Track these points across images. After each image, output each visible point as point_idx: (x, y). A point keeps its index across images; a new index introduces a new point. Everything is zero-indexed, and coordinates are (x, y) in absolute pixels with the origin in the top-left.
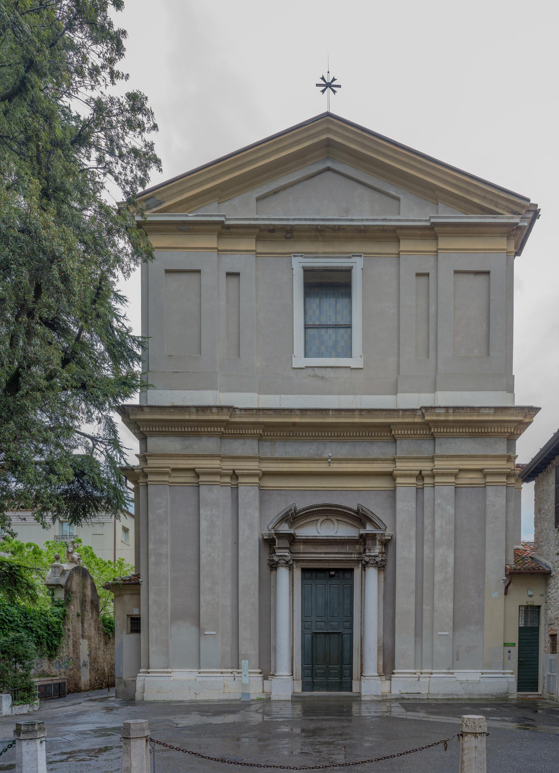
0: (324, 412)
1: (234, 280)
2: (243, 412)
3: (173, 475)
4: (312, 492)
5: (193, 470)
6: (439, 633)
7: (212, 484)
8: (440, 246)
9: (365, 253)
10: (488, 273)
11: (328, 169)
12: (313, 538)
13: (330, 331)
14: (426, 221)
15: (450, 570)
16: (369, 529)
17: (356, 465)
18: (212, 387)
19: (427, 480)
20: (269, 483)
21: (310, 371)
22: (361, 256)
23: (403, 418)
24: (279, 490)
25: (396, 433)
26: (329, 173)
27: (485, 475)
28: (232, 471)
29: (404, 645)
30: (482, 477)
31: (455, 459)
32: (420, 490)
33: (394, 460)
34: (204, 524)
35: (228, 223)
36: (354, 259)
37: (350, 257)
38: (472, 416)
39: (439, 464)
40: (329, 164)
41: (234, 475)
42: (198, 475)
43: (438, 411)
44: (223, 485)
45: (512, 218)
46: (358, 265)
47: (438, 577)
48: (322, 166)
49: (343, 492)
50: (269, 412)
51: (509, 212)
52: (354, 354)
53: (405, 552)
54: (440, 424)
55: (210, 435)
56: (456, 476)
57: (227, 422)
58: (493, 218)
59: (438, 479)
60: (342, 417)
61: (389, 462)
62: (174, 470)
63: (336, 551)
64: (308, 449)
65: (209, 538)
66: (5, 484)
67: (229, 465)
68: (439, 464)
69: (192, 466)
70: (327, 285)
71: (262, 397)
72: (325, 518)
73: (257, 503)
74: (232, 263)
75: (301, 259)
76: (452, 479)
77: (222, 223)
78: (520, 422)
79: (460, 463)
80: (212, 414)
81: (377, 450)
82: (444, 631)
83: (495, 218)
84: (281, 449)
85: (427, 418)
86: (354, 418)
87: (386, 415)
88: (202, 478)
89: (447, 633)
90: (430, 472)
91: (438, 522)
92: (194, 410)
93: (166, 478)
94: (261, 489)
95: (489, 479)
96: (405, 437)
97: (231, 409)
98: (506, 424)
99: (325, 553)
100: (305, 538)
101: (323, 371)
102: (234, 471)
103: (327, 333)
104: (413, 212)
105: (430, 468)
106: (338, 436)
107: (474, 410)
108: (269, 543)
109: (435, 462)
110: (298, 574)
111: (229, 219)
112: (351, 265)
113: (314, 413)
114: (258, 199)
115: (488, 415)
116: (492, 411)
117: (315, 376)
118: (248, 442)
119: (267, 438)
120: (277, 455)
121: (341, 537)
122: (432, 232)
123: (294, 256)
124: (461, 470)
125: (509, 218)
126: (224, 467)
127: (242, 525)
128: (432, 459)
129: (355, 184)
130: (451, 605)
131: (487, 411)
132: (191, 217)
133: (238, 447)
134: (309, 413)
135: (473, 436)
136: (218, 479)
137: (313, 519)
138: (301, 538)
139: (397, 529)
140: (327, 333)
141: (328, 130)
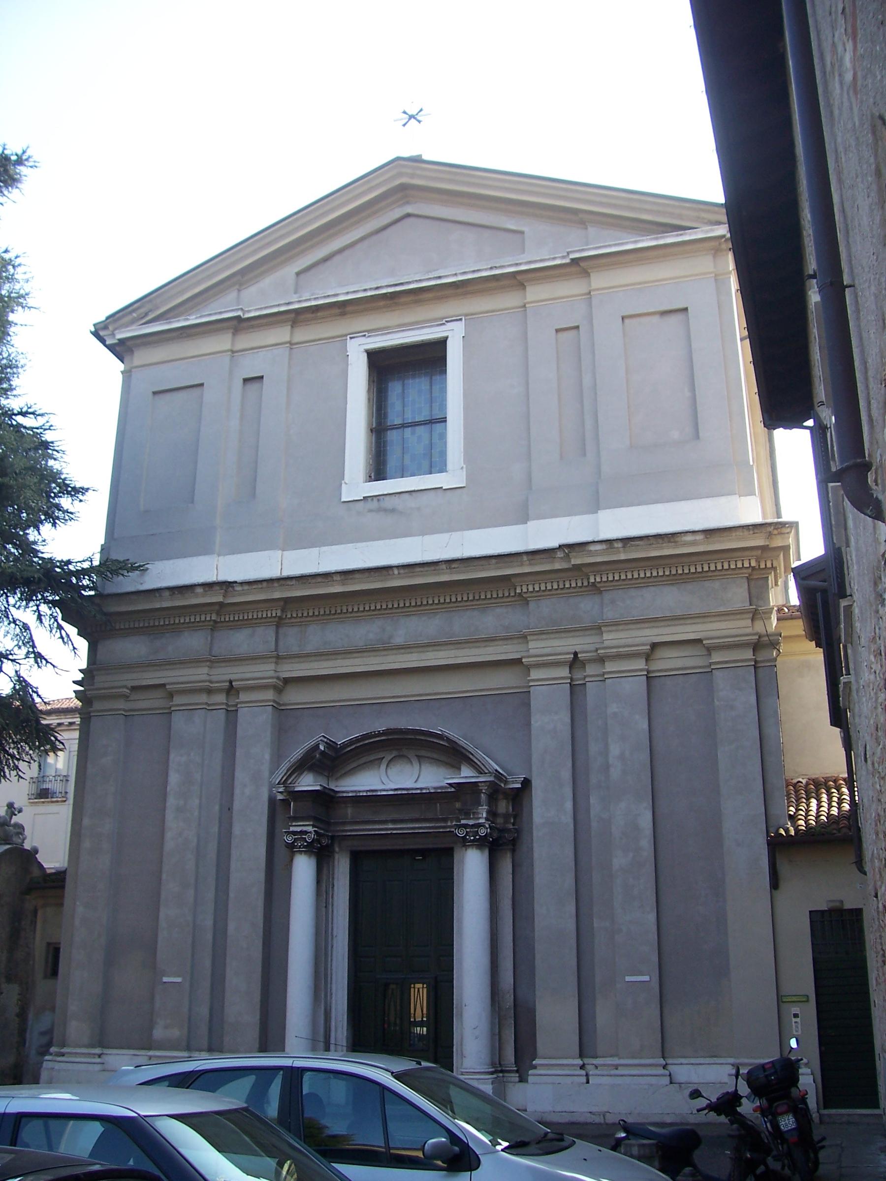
0: (384, 572)
1: (253, 387)
2: (246, 587)
3: (134, 696)
4: (374, 706)
5: (699, 641)
6: (628, 979)
7: (191, 709)
8: (594, 285)
9: (466, 315)
10: (686, 309)
11: (408, 215)
12: (369, 794)
13: (420, 430)
14: (563, 257)
15: (646, 843)
16: (466, 774)
17: (453, 653)
18: (205, 549)
19: (591, 670)
20: (296, 697)
21: (374, 504)
22: (461, 319)
23: (530, 564)
24: (314, 710)
25: (525, 590)
26: (411, 219)
27: (709, 650)
28: (228, 684)
29: (555, 1015)
30: (705, 653)
31: (643, 625)
32: (576, 690)
33: (524, 638)
34: (569, 805)
35: (247, 316)
36: (450, 326)
37: (444, 324)
38: (662, 548)
39: (612, 639)
40: (409, 209)
41: (231, 689)
42: (171, 695)
43: (592, 548)
44: (209, 708)
45: (712, 230)
46: (456, 337)
47: (619, 861)
48: (397, 213)
49: (623, 679)
50: (289, 582)
51: (706, 223)
52: (450, 466)
53: (548, 812)
54: (603, 568)
55: (194, 627)
56: (126, 697)
57: (221, 605)
58: (677, 235)
59: (610, 667)
60: (419, 576)
61: (515, 641)
62: (134, 688)
63: (416, 815)
64: (363, 632)
65: (182, 802)
66: (393, 986)
67: (223, 674)
68: (612, 639)
69: (162, 681)
70: (406, 368)
71: (290, 555)
72: (395, 753)
73: (267, 736)
74: (251, 366)
75: (363, 340)
76: (640, 664)
77: (238, 317)
78: (764, 548)
79: (655, 631)
80: (197, 595)
81: (489, 621)
82: (641, 974)
83: (681, 235)
84: (317, 636)
85: (573, 562)
86: (439, 574)
87: (497, 563)
88: (178, 700)
89: (647, 978)
90: (595, 654)
91: (615, 750)
92: (167, 594)
93: (121, 704)
94: (279, 709)
95: (716, 657)
96: (540, 595)
97: (227, 585)
98: (739, 554)
99: (394, 821)
100: (354, 794)
101: (395, 500)
102: (231, 682)
103: (413, 433)
104: (543, 247)
105: (592, 647)
106: (416, 606)
107: (663, 539)
108: (284, 806)
109: (604, 635)
110: (342, 867)
111: (249, 311)
112: (444, 334)
113: (367, 574)
114: (298, 274)
115: (694, 543)
116: (700, 537)
117: (380, 510)
118: (260, 630)
119: (293, 620)
120: (309, 649)
121: (421, 789)
122: (579, 267)
123: (351, 338)
124: (654, 646)
125: (707, 232)
126: (214, 678)
127: (241, 776)
128: (598, 629)
129: (450, 225)
130: (652, 917)
131: (689, 538)
132: (193, 320)
133: (241, 641)
134: (357, 576)
135: (675, 580)
136: (203, 698)
137: (372, 757)
138: (345, 795)
139: (534, 768)
140: (413, 433)
141: (400, 175)
